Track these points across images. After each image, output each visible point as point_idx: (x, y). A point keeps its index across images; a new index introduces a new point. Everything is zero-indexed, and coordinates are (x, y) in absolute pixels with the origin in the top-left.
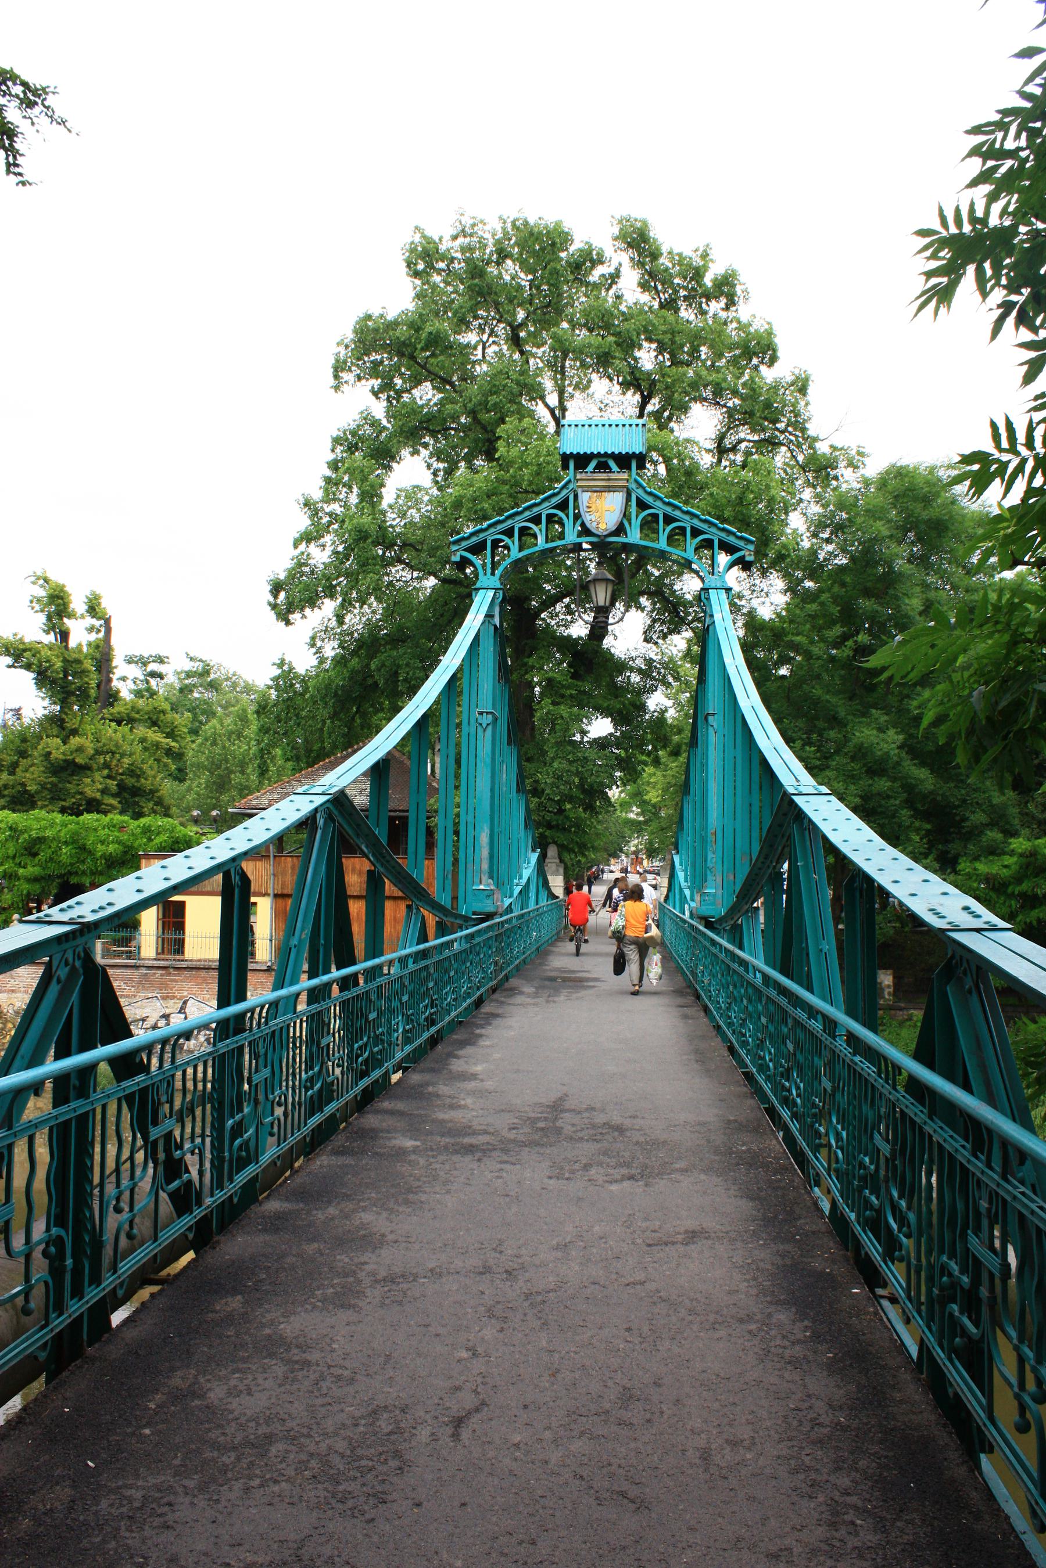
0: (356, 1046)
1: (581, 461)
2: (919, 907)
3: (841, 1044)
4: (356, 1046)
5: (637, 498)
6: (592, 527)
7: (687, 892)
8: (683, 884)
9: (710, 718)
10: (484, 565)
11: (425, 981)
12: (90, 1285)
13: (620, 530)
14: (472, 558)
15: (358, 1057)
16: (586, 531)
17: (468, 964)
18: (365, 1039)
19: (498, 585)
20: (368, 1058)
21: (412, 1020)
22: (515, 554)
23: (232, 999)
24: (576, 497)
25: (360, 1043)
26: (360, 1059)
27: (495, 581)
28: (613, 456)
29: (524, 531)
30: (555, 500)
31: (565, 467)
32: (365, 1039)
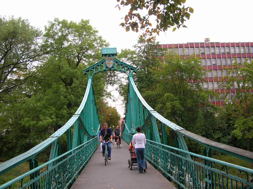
0: (65, 175)
1: (106, 55)
2: (173, 128)
3: (189, 159)
4: (65, 175)
5: (116, 61)
6: (108, 66)
7: (128, 130)
8: (127, 129)
9: (131, 99)
10: (89, 74)
11: (79, 155)
12: (35, 177)
13: (113, 67)
14: (87, 73)
15: (65, 178)
16: (107, 67)
17: (88, 150)
18: (67, 173)
19: (92, 78)
20: (68, 178)
21: (77, 165)
22: (95, 72)
23: (34, 167)
24: (105, 61)
25: (66, 174)
26: (66, 179)
27: (91, 77)
28: (111, 54)
29: (96, 68)
30: (86, 70)
31: (103, 56)
32: (67, 173)
